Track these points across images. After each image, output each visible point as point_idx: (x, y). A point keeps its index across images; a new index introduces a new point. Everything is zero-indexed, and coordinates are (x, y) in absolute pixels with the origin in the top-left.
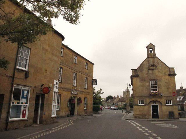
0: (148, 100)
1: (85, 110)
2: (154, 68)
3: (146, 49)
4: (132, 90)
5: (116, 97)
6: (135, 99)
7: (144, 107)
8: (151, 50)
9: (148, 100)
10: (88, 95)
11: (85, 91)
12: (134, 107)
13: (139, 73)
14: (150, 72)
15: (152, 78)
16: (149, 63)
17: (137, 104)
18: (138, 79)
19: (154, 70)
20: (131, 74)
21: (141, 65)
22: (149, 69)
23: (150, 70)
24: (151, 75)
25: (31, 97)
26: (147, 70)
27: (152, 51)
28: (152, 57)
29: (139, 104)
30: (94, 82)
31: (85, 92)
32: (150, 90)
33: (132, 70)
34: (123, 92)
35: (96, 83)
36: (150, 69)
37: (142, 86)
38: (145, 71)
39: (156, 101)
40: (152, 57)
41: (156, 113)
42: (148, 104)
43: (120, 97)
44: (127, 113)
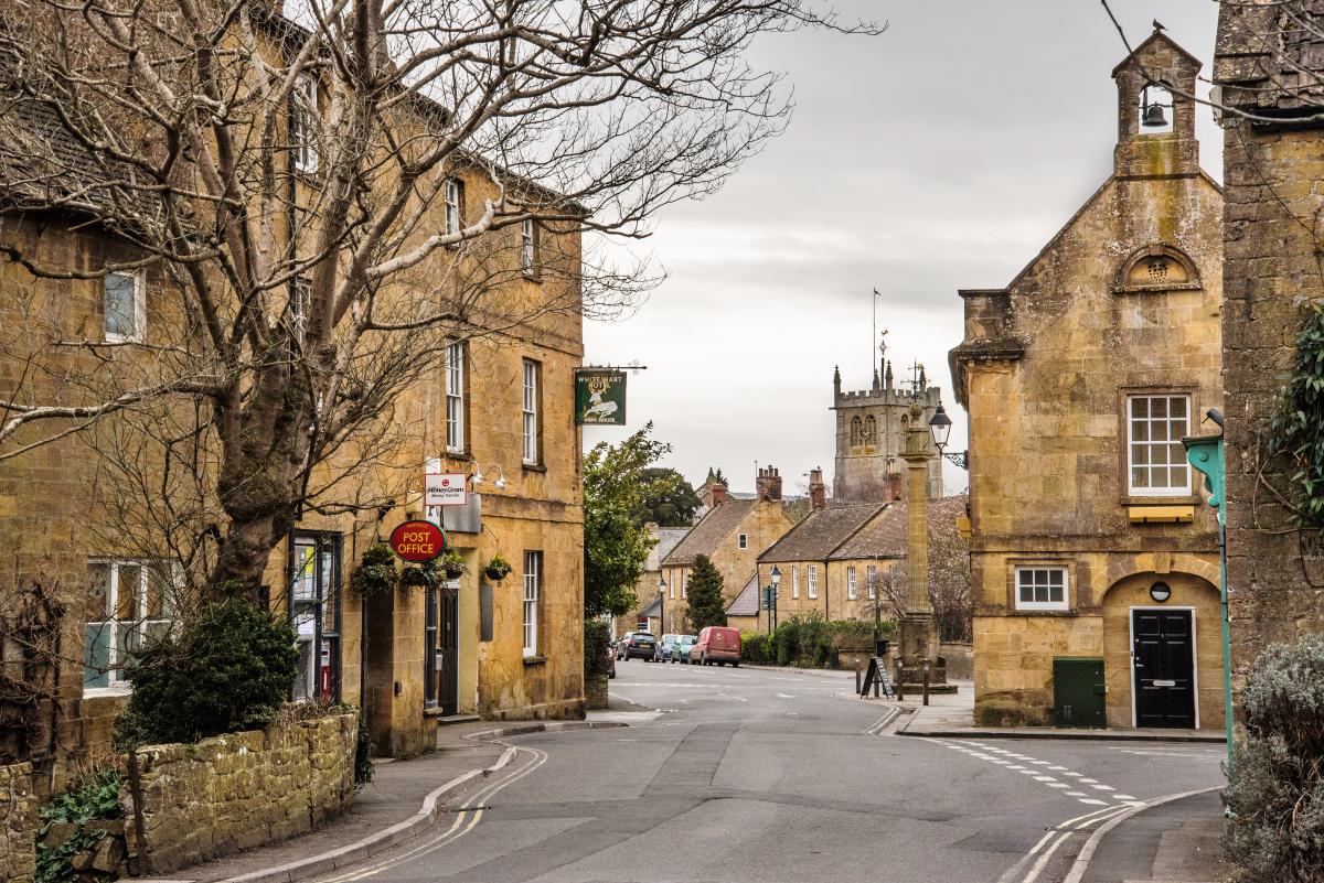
0: (1100, 570)
1: (528, 664)
2: (1174, 274)
3: (1112, 89)
4: (966, 465)
5: (743, 484)
6: (988, 559)
7: (1062, 624)
8: (1158, 96)
9: (1100, 570)
10: (546, 528)
11: (525, 494)
12: (983, 628)
13: (1026, 325)
14: (1133, 315)
15: (1149, 371)
16: (1124, 231)
17: (1000, 607)
18: (1015, 380)
19: (1170, 298)
20: (956, 337)
21: (1045, 252)
22: (1120, 291)
23: (1126, 301)
24: (1134, 350)
25: (1203, 720)
26: (1104, 295)
27: (1168, 114)
28: (1163, 177)
29: (1020, 606)
30: (596, 397)
31: (524, 502)
32: (1122, 480)
33: (962, 293)
34: (843, 402)
35: (612, 407)
36: (1132, 294)
37: (1053, 443)
38: (1086, 302)
39: (1175, 575)
40: (1163, 177)
41: (1171, 683)
42: (1097, 599)
43: (794, 487)
44: (913, 700)
